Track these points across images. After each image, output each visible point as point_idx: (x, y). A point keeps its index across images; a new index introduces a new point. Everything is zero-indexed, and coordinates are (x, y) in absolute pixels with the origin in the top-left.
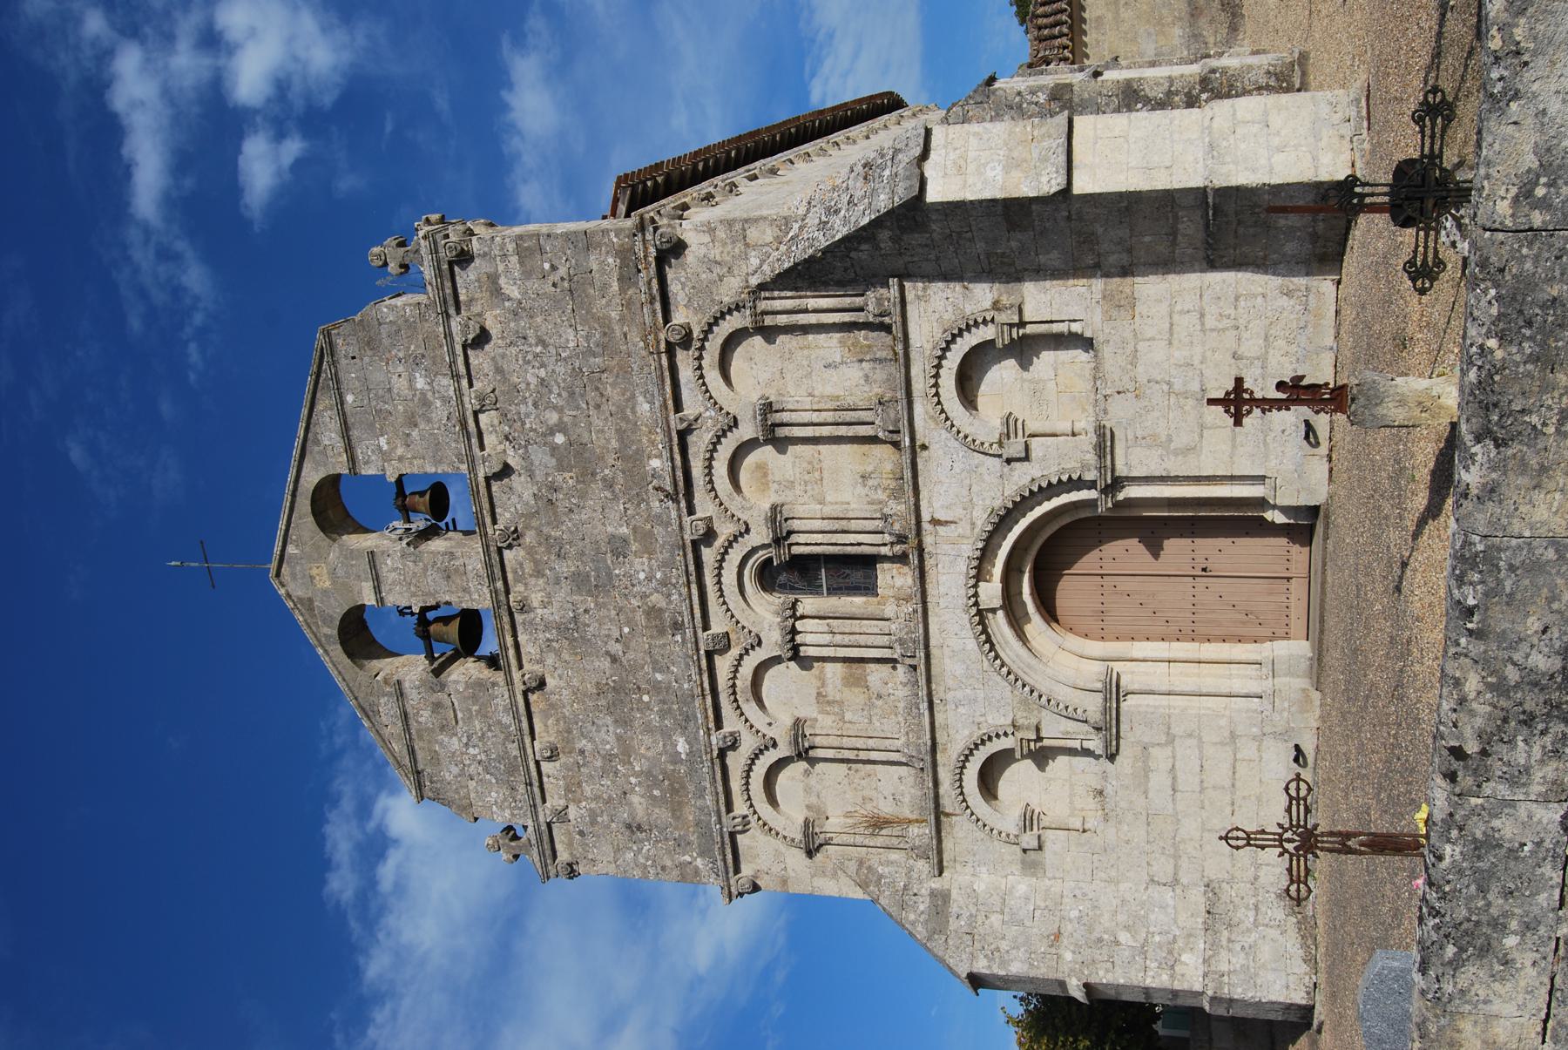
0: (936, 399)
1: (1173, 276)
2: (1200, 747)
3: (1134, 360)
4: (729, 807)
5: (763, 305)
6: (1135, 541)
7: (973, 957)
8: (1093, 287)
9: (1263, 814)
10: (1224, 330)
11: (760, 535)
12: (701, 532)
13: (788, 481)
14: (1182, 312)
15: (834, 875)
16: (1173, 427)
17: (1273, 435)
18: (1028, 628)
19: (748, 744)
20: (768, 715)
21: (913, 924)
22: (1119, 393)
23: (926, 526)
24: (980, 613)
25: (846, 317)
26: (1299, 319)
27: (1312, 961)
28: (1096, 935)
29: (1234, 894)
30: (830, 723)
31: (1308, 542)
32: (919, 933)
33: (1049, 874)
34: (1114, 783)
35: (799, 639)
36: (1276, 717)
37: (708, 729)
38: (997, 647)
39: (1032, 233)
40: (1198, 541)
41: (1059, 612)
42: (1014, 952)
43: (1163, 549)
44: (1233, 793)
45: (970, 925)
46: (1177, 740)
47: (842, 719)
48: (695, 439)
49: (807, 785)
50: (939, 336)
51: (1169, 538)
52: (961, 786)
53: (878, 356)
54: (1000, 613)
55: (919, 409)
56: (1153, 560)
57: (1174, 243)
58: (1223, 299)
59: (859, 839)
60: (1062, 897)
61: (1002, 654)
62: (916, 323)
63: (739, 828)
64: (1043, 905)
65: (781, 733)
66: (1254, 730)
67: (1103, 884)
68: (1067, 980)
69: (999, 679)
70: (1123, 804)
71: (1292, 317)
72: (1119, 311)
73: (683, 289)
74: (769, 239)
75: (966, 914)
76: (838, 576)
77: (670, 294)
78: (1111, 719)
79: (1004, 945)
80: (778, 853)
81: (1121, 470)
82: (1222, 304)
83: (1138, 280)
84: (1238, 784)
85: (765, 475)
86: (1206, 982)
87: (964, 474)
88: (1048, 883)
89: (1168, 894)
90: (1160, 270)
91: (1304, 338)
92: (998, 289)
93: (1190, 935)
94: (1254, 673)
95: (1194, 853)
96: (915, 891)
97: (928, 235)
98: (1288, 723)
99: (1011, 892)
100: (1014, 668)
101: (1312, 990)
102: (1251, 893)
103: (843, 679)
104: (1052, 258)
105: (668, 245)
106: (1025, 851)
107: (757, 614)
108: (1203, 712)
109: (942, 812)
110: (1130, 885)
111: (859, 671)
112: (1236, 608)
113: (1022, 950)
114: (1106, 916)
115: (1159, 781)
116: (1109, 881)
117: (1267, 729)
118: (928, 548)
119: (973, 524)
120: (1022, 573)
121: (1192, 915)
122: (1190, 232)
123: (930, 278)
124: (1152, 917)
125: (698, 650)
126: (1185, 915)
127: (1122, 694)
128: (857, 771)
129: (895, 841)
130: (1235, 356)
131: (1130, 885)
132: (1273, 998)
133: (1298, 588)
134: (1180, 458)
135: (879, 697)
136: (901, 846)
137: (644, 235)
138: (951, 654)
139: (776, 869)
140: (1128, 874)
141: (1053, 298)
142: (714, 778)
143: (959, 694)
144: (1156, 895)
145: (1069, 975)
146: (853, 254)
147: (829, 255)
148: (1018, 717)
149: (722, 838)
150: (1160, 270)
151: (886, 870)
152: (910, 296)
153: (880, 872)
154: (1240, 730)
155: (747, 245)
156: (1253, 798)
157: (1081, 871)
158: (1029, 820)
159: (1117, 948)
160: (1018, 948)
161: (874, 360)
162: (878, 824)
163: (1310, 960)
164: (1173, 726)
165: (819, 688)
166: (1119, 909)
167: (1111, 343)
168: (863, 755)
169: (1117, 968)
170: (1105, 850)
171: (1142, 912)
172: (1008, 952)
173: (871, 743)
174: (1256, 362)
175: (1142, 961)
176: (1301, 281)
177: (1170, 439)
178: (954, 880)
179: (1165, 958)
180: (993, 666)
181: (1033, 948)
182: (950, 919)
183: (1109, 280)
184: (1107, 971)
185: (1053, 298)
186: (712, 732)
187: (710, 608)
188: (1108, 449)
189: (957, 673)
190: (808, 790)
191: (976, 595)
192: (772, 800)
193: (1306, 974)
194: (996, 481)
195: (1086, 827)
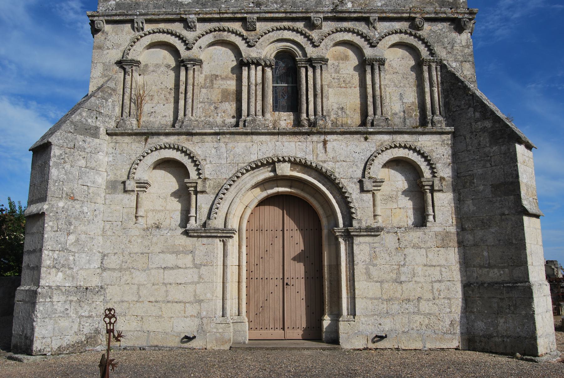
0: (393, 146)
1: (459, 267)
2: (192, 283)
3: (416, 247)
4: (149, 21)
5: (434, 65)
6: (302, 248)
7: (61, 147)
8: (452, 227)
9: (150, 319)
10: (433, 292)
11: (311, 52)
12: (315, 22)
13: (339, 71)
14: (441, 271)
15: (104, 76)
16: (381, 267)
17: (378, 319)
18: (258, 190)
19: (189, 35)
20: (205, 48)
21: (80, 114)
22: (399, 239)
23: (322, 137)
24: (274, 163)
25: (429, 106)
26: (439, 329)
27: (60, 351)
28: (73, 221)
29: (97, 303)
30: (200, 81)
31: (305, 338)
32: (75, 117)
33: (108, 196)
34: (169, 234)
35: (253, 67)
36: (213, 325)
37: (199, 14)
38: (252, 172)
39: (490, 196)
40: (303, 281)
41: (267, 208)
42: (64, 172)
43: (298, 262)
44: (163, 302)
45: (79, 147)
46: (196, 270)
47: (202, 87)
48: (363, 26)
49: (160, 66)
50: (425, 150)
51: (304, 265)
52: (166, 148)
53: (407, 120)
54: (272, 174)
55: (386, 137)
56: (291, 258)
57: (481, 267)
58: (448, 292)
59: (128, 90)
60: (95, 203)
61: (248, 174)
62: (431, 139)
63: (136, 25)
64: (91, 191)
65: (195, 53)
66: (205, 313)
67: (102, 227)
68: (47, 202)
69: (234, 171)
70: (155, 240)
71: (440, 326)
72: (441, 240)
73: (439, 29)
74: (465, 73)
75: (86, 146)
76: (283, 92)
77: (436, 23)
78: (211, 233)
79: (67, 166)
80: (119, 46)
81: (357, 240)
82: (446, 291)
83: (456, 250)
84: (169, 305)
85: (342, 59)
86: (45, 287)
87: (352, 159)
88: (103, 195)
89: (97, 264)
90: (462, 260)
91: (429, 333)
92: (449, 180)
93: (73, 278)
94: (234, 312)
95: (123, 280)
96: (99, 118)
97: (488, 145)
98: (209, 332)
99: (98, 173)
100: (239, 180)
101: (42, 353)
102: (98, 313)
103: (226, 89)
104: (469, 206)
105: (463, 24)
106: (124, 183)
107: (267, 46)
108: (214, 284)
109: (148, 137)
110: (101, 243)
111: (231, 98)
112: (265, 302)
113: (65, 177)
114: (84, 228)
115: (170, 259)
116: (104, 231)
117: (205, 321)
118: (310, 138)
119: (325, 162)
120: (290, 187)
121: (84, 279)
122: (491, 275)
123: (454, 147)
124: (84, 255)
125: (247, 13)
126: (85, 274)
127: (224, 239)
128: (170, 93)
129: (127, 110)
130: (419, 298)
131: (101, 243)
132: (37, 330)
133: (279, 333)
134: (365, 271)
135: (216, 108)
136: (124, 114)
137: (467, 14)
138: (248, 147)
139: (108, 44)
140: (108, 241)
141: (446, 207)
142: (169, 14)
143: (223, 150)
144: (96, 258)
145: (50, 204)
146: (471, 109)
147: (471, 97)
148: (210, 181)
149: (130, 15)
150: (462, 260)
151: (110, 104)
152: (444, 137)
153: (109, 100)
154: (204, 305)
155: (462, 62)
156: (160, 313)
157: (110, 215)
158: (143, 185)
159: (65, 233)
160: (66, 174)
161: (405, 118)
162: (138, 102)
163: (60, 351)
164: (206, 267)
165: (221, 76)
166: (88, 236)
167: (424, 236)
168: (182, 96)
169: (54, 233)
170: (124, 229)
171: (86, 249)
172: (64, 168)
173: (189, 101)
174: (417, 309)
175: (58, 249)
176: (458, 330)
177: (375, 265)
178: (104, 142)
179: (60, 263)
180: (243, 168)
181: (66, 183)
182: (83, 136)
183: (456, 235)
184: (52, 227)
185: (446, 207)
186: (197, 16)
187: (269, 23)
188: (370, 233)
189: (236, 149)
190: (157, 66)
191: (284, 161)
192: (152, 45)
193: (52, 348)
194: (349, 175)
195: (139, 218)
